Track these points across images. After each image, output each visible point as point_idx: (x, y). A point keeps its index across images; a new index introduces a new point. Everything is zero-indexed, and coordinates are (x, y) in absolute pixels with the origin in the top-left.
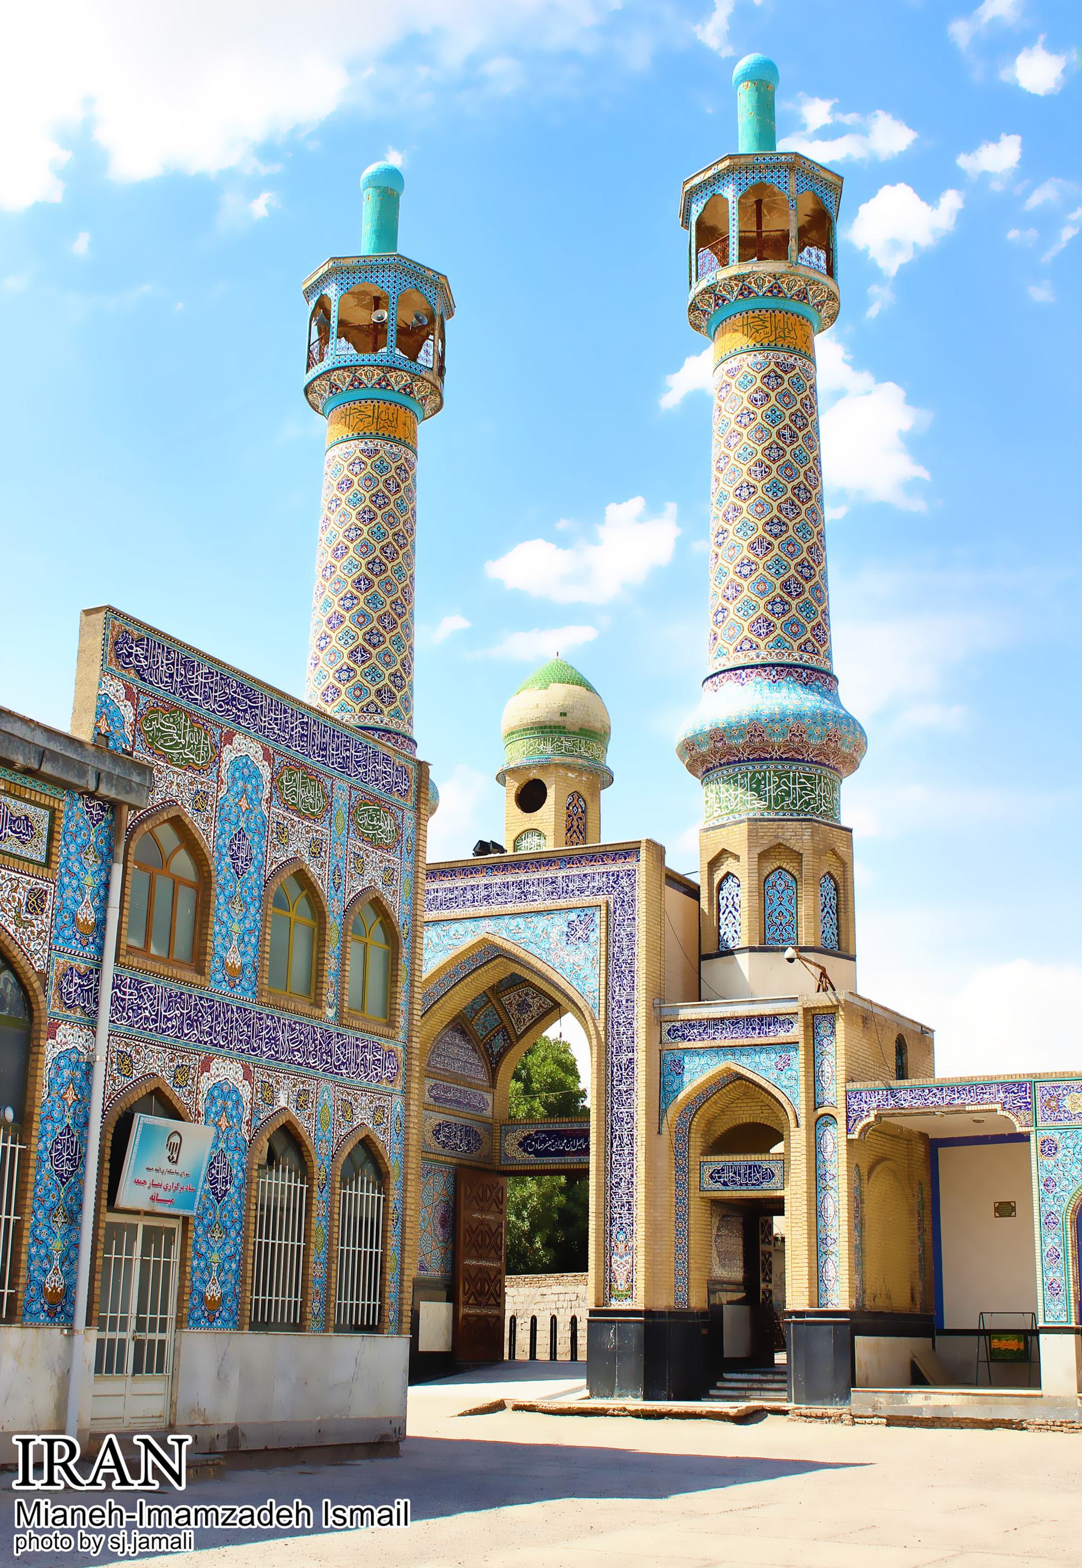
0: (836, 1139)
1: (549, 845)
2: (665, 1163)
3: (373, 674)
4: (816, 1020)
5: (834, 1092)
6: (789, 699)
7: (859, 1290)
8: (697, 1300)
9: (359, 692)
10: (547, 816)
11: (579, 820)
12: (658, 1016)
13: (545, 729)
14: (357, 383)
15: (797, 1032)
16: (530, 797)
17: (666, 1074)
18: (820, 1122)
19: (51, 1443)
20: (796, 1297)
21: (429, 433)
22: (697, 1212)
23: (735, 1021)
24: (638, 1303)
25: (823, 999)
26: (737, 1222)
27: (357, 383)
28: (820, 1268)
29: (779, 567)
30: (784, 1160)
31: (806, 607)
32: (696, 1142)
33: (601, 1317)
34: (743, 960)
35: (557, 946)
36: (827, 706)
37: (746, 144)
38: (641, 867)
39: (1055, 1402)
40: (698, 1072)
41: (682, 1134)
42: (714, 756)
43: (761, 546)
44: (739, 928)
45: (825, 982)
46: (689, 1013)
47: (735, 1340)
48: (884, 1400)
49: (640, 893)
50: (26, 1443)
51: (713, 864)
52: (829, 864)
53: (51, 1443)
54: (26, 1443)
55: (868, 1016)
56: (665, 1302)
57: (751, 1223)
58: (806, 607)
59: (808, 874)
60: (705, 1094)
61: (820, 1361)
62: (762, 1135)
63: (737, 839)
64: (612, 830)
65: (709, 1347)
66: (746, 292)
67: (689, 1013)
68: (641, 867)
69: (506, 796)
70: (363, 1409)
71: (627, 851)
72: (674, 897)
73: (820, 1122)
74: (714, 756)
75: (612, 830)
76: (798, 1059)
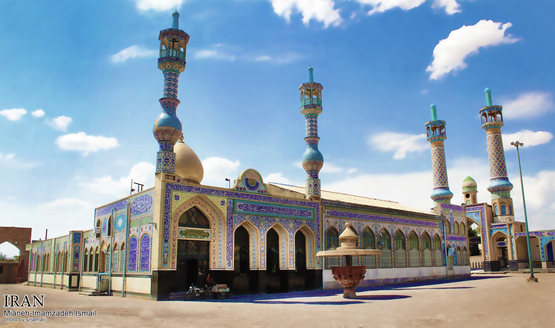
0: (513, 240)
1: (471, 204)
2: (491, 243)
3: (443, 180)
4: (510, 225)
5: (513, 234)
6: (503, 182)
7: (518, 257)
8: (497, 260)
9: (441, 182)
10: (470, 198)
11: (474, 199)
12: (489, 225)
13: (468, 187)
14: (435, 139)
15: (507, 226)
16: (467, 196)
17: (491, 232)
18: (511, 238)
19: (12, 296)
20: (510, 258)
21: (445, 142)
22: (496, 248)
23: (499, 225)
24: (489, 260)
25: (510, 222)
26: (501, 250)
27: (435, 139)
28: (512, 255)
29: (499, 164)
30: (507, 242)
31: (503, 169)
32: (495, 240)
33: (485, 263)
34: (499, 217)
35: (471, 215)
36: (508, 183)
37: (488, 105)
38: (484, 206)
39: (544, 270)
40: (494, 232)
41: (493, 240)
42: (493, 190)
43: (496, 161)
44: (498, 213)
45: (510, 220)
46: (493, 224)
47: (502, 264)
48: (522, 270)
49: (485, 210)
50: (6, 296)
51: (494, 204)
52: (509, 203)
53: (12, 296)
54: (6, 296)
55: (516, 223)
56: (493, 260)
57: (504, 250)
58: (503, 169)
59: (507, 206)
60: (496, 234)
61: (514, 266)
62: (503, 239)
63: (497, 201)
64: (479, 202)
65: (498, 265)
66: (490, 126)
67: (493, 224)
68: (484, 206)
69: (463, 196)
70: (467, 273)
71: (483, 204)
72: (488, 208)
73: (511, 238)
74: (493, 190)
75: (479, 202)
76: (508, 229)
